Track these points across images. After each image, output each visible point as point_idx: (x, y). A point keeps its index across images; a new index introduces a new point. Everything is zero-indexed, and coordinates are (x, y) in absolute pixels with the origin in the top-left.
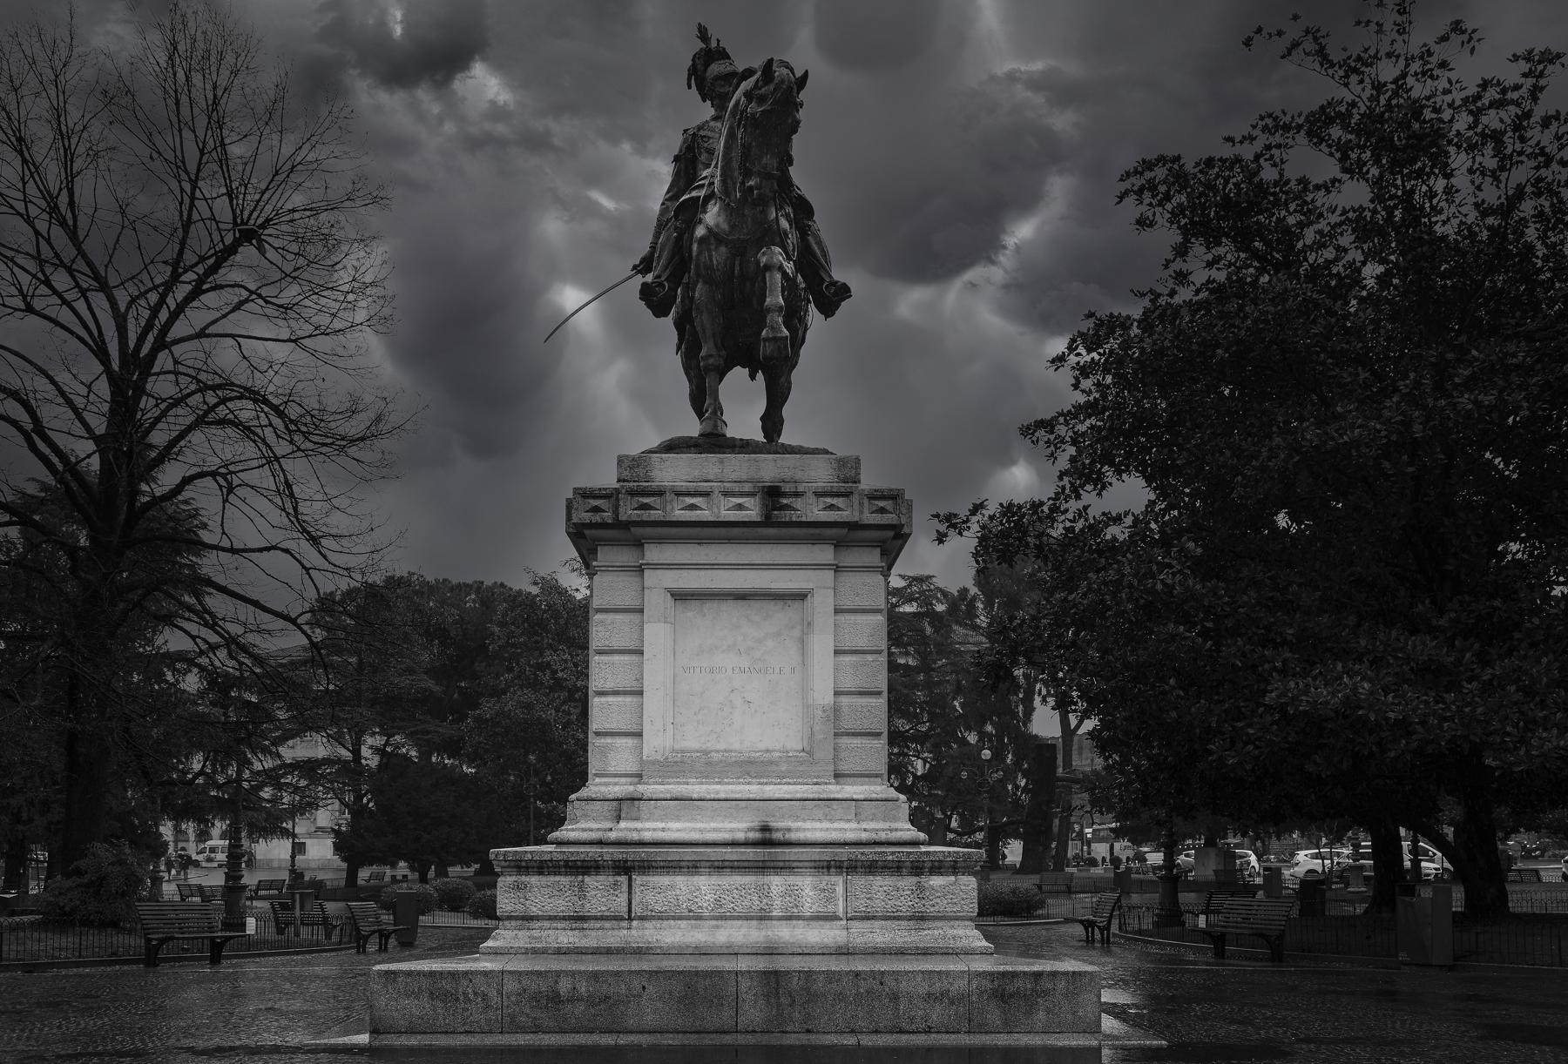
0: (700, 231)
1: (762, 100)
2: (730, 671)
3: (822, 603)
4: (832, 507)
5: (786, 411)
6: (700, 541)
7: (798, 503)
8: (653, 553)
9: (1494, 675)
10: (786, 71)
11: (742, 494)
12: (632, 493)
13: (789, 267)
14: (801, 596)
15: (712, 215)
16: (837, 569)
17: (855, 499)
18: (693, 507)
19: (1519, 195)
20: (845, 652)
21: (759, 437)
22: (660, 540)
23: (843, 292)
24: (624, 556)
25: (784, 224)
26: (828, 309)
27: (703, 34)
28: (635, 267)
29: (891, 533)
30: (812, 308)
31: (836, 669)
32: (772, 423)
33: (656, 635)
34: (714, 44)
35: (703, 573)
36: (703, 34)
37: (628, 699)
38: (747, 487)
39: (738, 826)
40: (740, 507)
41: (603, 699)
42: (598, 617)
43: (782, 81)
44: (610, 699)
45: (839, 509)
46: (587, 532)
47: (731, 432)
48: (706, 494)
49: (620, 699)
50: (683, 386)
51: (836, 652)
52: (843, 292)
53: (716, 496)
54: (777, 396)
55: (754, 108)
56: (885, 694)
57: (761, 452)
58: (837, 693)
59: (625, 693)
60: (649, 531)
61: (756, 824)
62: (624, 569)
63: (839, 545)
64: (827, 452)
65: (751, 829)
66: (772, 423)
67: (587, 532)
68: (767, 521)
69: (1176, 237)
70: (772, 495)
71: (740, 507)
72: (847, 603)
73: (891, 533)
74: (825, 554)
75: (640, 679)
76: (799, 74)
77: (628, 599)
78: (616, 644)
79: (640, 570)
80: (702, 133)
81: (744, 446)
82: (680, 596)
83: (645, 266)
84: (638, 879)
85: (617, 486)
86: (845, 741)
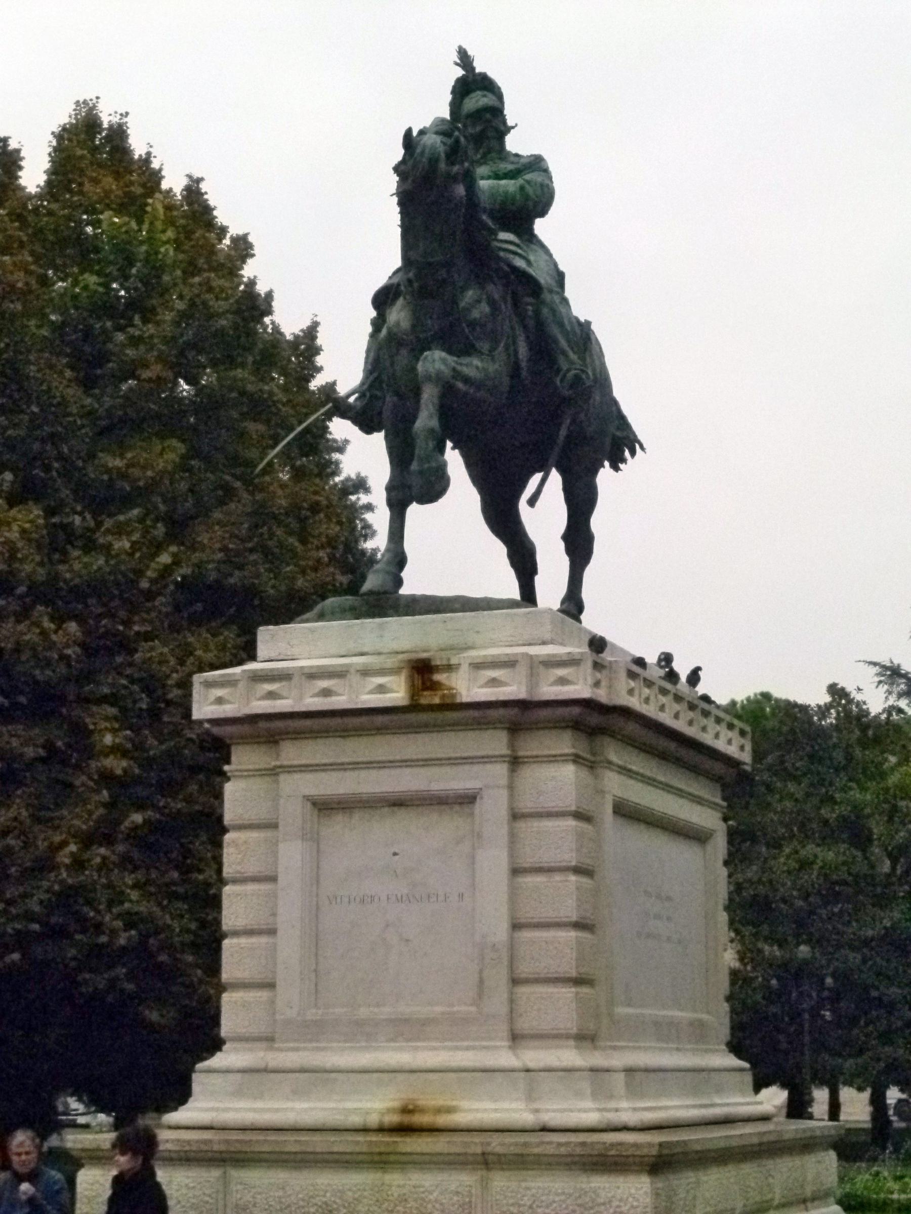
2: (384, 898)
3: (494, 808)
4: (494, 682)
5: (598, 522)
6: (345, 733)
8: (292, 752)
9: (114, 933)
11: (382, 672)
14: (468, 800)
19: (213, 561)
22: (298, 735)
27: (465, 60)
36: (465, 60)
38: (390, 662)
39: (375, 1105)
40: (381, 689)
49: (254, 940)
58: (516, 926)
59: (559, 925)
60: (279, 724)
61: (397, 1104)
65: (389, 1111)
70: (422, 671)
71: (381, 689)
74: (496, 742)
82: (325, 807)
84: (236, 1174)
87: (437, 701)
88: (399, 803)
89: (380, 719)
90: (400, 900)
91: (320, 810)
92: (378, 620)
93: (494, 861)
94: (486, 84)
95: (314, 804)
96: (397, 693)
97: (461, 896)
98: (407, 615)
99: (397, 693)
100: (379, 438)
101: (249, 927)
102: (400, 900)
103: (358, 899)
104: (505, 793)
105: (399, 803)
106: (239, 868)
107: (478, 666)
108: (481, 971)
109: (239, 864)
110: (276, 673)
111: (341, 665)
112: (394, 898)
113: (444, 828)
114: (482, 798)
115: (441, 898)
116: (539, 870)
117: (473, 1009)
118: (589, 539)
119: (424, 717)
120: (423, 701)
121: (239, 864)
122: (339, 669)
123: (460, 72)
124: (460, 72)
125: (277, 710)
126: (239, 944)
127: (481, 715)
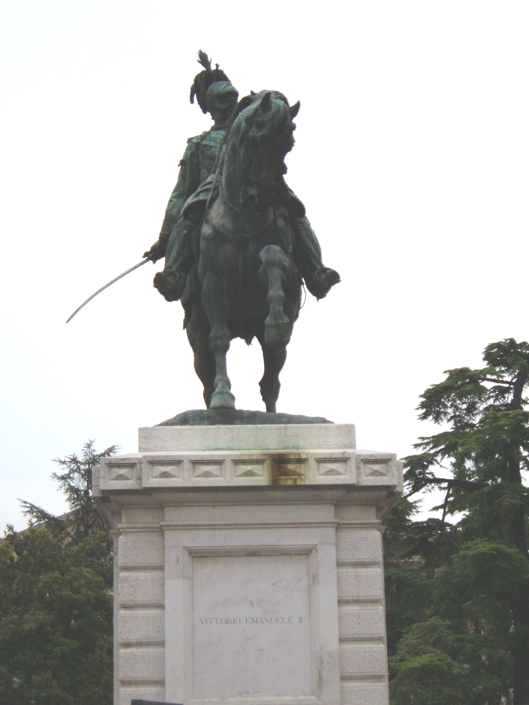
0: (206, 230)
1: (260, 126)
2: (243, 621)
3: (326, 557)
5: (283, 376)
6: (215, 504)
7: (302, 469)
8: (173, 516)
10: (282, 103)
12: (154, 462)
13: (287, 262)
15: (217, 213)
16: (339, 527)
17: (352, 463)
18: (207, 474)
20: (347, 602)
21: (262, 407)
22: (178, 504)
23: (333, 278)
24: (146, 518)
25: (281, 223)
26: (319, 292)
27: (204, 59)
28: (146, 254)
29: (385, 493)
30: (304, 289)
31: (340, 618)
32: (270, 388)
33: (175, 590)
34: (213, 67)
35: (217, 533)
36: (204, 59)
37: (151, 650)
40: (250, 474)
41: (129, 650)
42: (123, 574)
43: (278, 111)
44: (134, 650)
45: (338, 473)
46: (112, 498)
47: (239, 405)
48: (219, 462)
50: (186, 355)
51: (341, 602)
52: (333, 278)
53: (228, 465)
54: (274, 359)
55: (256, 133)
56: (383, 602)
57: (265, 423)
58: (342, 640)
60: (168, 496)
62: (147, 530)
63: (338, 504)
64: (324, 421)
66: (270, 388)
67: (112, 498)
68: (274, 486)
69: (441, 502)
70: (280, 463)
72: (348, 557)
73: (385, 493)
74: (326, 513)
75: (161, 630)
76: (292, 103)
77: (151, 558)
78: (140, 598)
79: (161, 531)
80: (205, 142)
81: (251, 418)
82: (197, 555)
83: (153, 255)
85: (140, 455)
86: (350, 685)
87: (290, 483)
88: (253, 553)
89: (220, 496)
90: (255, 621)
91: (193, 557)
92: (229, 426)
93: (327, 594)
94: (220, 76)
95: (190, 553)
96: (261, 477)
97: (301, 620)
98: (249, 423)
99: (261, 477)
100: (177, 305)
101: (139, 640)
102: (255, 621)
103: (223, 621)
104: (333, 548)
105: (253, 553)
106: (131, 598)
107: (320, 461)
108: (320, 672)
109: (131, 595)
110: (156, 459)
111: (219, 456)
112: (251, 620)
113: (289, 572)
114: (317, 552)
115: (286, 620)
116: (357, 602)
117: (313, 698)
118: (277, 386)
119: (279, 494)
120: (282, 483)
121: (131, 595)
122: (218, 458)
123: (202, 68)
124: (202, 68)
125: (209, 485)
126: (132, 653)
127: (319, 493)
